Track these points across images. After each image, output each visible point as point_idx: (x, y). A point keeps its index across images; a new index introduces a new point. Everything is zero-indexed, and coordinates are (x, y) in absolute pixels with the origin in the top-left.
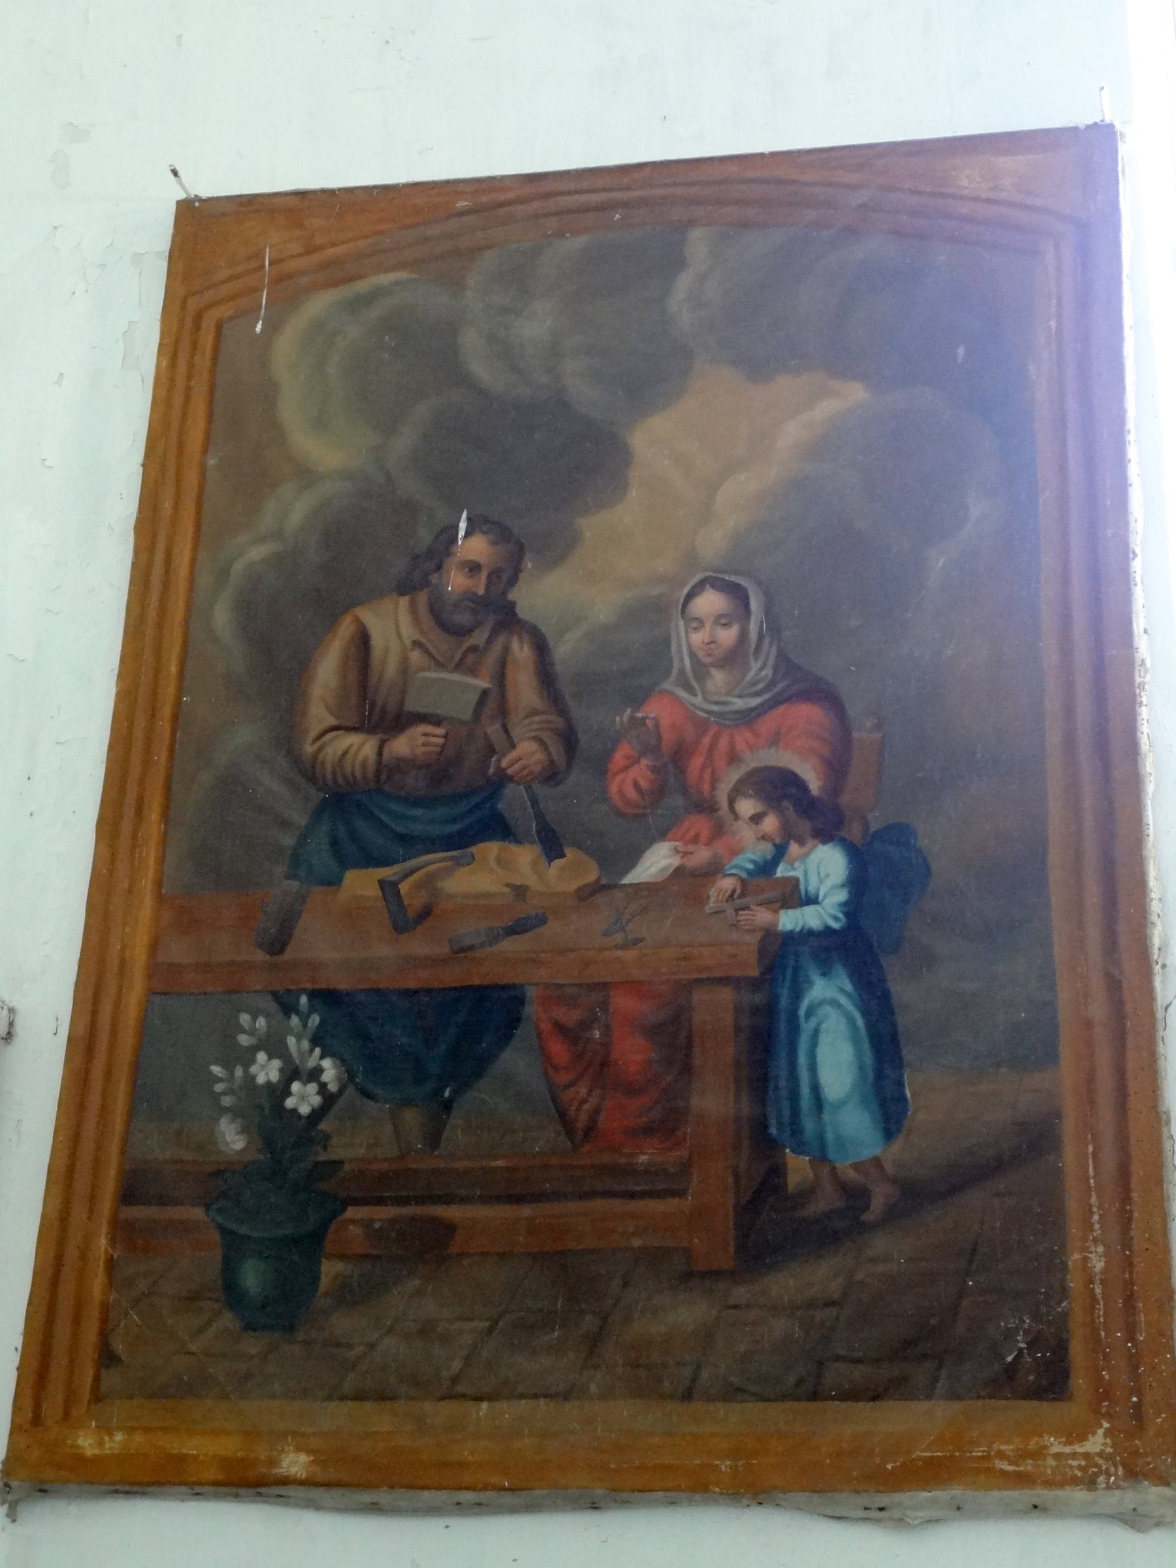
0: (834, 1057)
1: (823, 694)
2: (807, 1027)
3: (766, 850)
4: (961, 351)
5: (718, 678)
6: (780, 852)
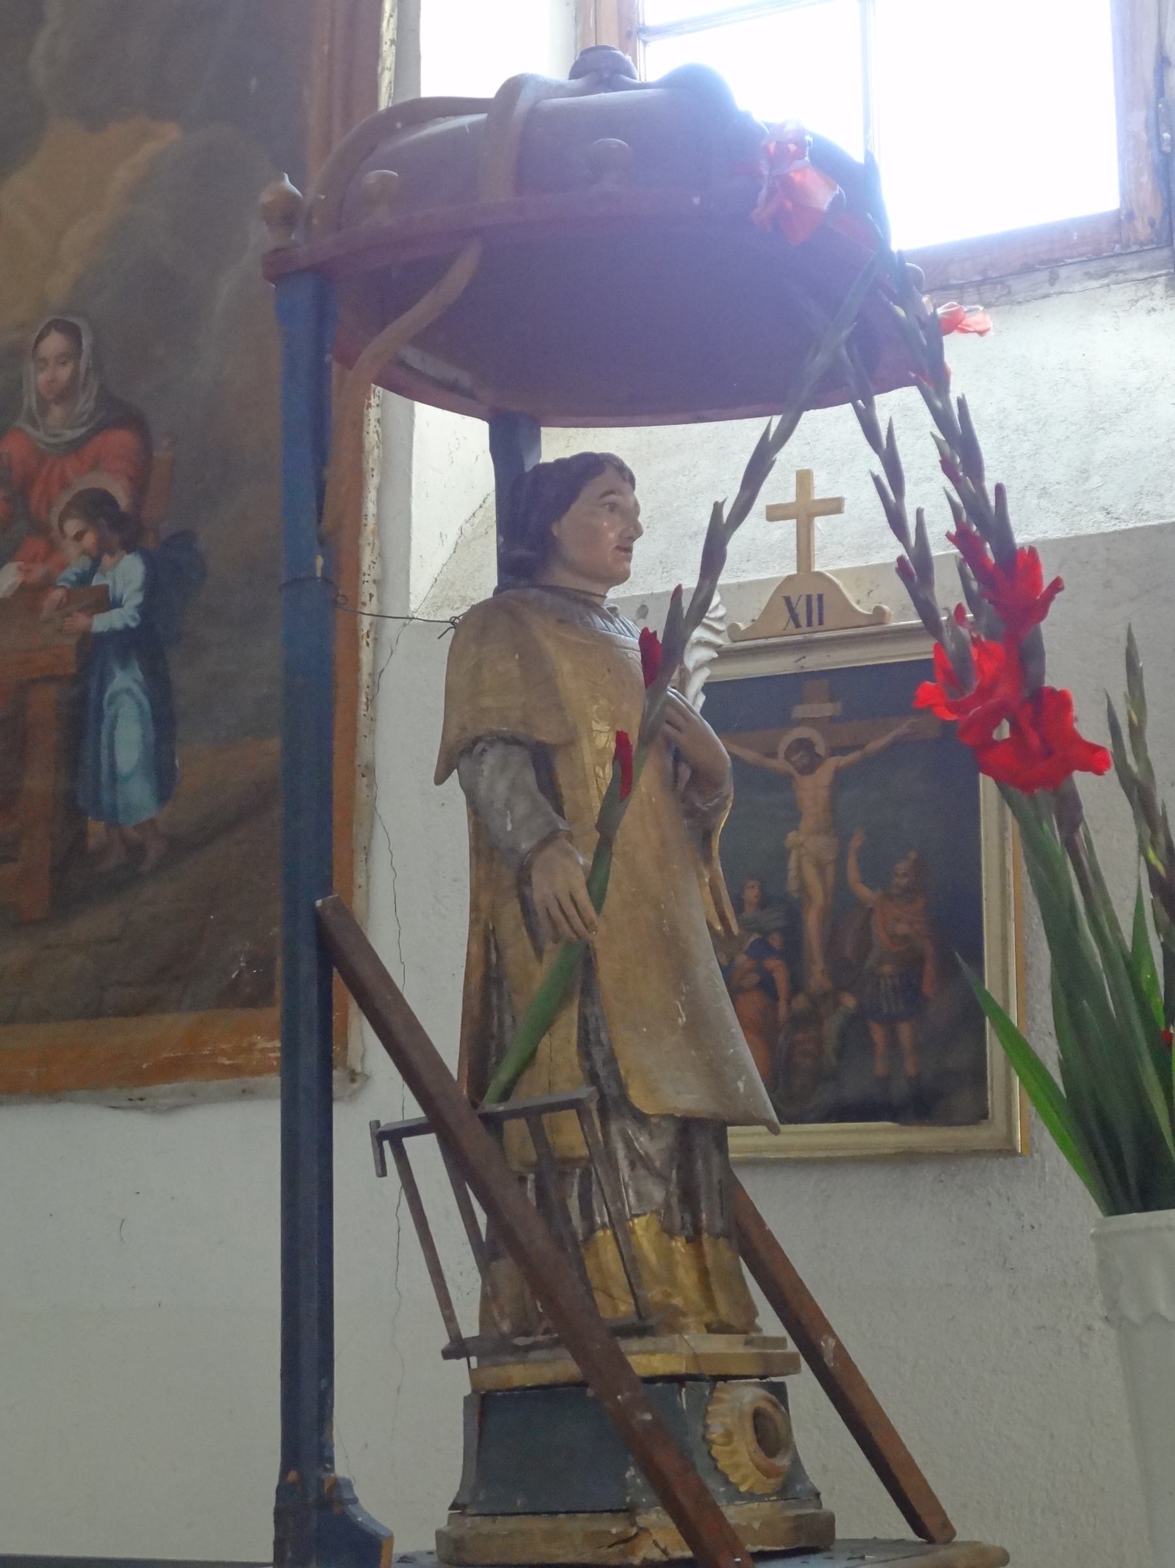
0: (128, 740)
1: (135, 421)
2: (108, 712)
3: (83, 564)
4: (253, 83)
5: (57, 412)
6: (96, 563)
